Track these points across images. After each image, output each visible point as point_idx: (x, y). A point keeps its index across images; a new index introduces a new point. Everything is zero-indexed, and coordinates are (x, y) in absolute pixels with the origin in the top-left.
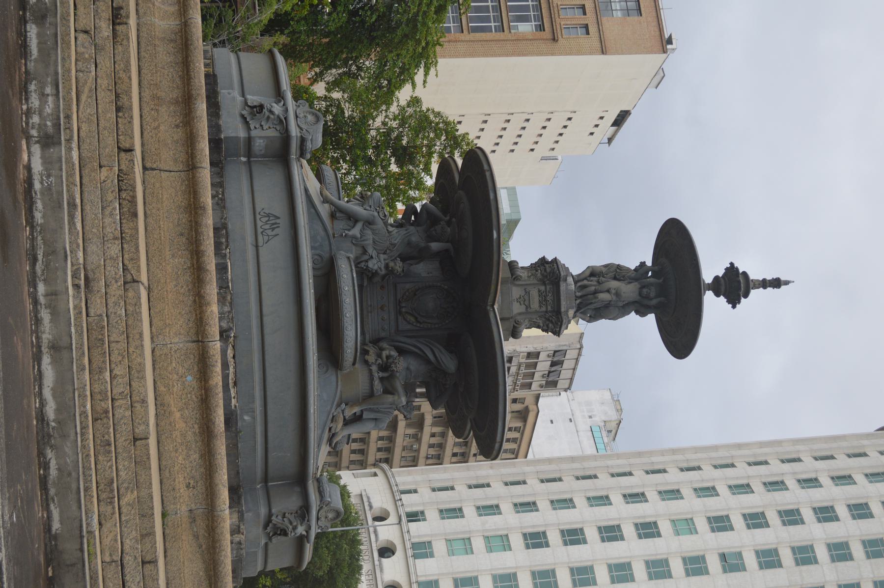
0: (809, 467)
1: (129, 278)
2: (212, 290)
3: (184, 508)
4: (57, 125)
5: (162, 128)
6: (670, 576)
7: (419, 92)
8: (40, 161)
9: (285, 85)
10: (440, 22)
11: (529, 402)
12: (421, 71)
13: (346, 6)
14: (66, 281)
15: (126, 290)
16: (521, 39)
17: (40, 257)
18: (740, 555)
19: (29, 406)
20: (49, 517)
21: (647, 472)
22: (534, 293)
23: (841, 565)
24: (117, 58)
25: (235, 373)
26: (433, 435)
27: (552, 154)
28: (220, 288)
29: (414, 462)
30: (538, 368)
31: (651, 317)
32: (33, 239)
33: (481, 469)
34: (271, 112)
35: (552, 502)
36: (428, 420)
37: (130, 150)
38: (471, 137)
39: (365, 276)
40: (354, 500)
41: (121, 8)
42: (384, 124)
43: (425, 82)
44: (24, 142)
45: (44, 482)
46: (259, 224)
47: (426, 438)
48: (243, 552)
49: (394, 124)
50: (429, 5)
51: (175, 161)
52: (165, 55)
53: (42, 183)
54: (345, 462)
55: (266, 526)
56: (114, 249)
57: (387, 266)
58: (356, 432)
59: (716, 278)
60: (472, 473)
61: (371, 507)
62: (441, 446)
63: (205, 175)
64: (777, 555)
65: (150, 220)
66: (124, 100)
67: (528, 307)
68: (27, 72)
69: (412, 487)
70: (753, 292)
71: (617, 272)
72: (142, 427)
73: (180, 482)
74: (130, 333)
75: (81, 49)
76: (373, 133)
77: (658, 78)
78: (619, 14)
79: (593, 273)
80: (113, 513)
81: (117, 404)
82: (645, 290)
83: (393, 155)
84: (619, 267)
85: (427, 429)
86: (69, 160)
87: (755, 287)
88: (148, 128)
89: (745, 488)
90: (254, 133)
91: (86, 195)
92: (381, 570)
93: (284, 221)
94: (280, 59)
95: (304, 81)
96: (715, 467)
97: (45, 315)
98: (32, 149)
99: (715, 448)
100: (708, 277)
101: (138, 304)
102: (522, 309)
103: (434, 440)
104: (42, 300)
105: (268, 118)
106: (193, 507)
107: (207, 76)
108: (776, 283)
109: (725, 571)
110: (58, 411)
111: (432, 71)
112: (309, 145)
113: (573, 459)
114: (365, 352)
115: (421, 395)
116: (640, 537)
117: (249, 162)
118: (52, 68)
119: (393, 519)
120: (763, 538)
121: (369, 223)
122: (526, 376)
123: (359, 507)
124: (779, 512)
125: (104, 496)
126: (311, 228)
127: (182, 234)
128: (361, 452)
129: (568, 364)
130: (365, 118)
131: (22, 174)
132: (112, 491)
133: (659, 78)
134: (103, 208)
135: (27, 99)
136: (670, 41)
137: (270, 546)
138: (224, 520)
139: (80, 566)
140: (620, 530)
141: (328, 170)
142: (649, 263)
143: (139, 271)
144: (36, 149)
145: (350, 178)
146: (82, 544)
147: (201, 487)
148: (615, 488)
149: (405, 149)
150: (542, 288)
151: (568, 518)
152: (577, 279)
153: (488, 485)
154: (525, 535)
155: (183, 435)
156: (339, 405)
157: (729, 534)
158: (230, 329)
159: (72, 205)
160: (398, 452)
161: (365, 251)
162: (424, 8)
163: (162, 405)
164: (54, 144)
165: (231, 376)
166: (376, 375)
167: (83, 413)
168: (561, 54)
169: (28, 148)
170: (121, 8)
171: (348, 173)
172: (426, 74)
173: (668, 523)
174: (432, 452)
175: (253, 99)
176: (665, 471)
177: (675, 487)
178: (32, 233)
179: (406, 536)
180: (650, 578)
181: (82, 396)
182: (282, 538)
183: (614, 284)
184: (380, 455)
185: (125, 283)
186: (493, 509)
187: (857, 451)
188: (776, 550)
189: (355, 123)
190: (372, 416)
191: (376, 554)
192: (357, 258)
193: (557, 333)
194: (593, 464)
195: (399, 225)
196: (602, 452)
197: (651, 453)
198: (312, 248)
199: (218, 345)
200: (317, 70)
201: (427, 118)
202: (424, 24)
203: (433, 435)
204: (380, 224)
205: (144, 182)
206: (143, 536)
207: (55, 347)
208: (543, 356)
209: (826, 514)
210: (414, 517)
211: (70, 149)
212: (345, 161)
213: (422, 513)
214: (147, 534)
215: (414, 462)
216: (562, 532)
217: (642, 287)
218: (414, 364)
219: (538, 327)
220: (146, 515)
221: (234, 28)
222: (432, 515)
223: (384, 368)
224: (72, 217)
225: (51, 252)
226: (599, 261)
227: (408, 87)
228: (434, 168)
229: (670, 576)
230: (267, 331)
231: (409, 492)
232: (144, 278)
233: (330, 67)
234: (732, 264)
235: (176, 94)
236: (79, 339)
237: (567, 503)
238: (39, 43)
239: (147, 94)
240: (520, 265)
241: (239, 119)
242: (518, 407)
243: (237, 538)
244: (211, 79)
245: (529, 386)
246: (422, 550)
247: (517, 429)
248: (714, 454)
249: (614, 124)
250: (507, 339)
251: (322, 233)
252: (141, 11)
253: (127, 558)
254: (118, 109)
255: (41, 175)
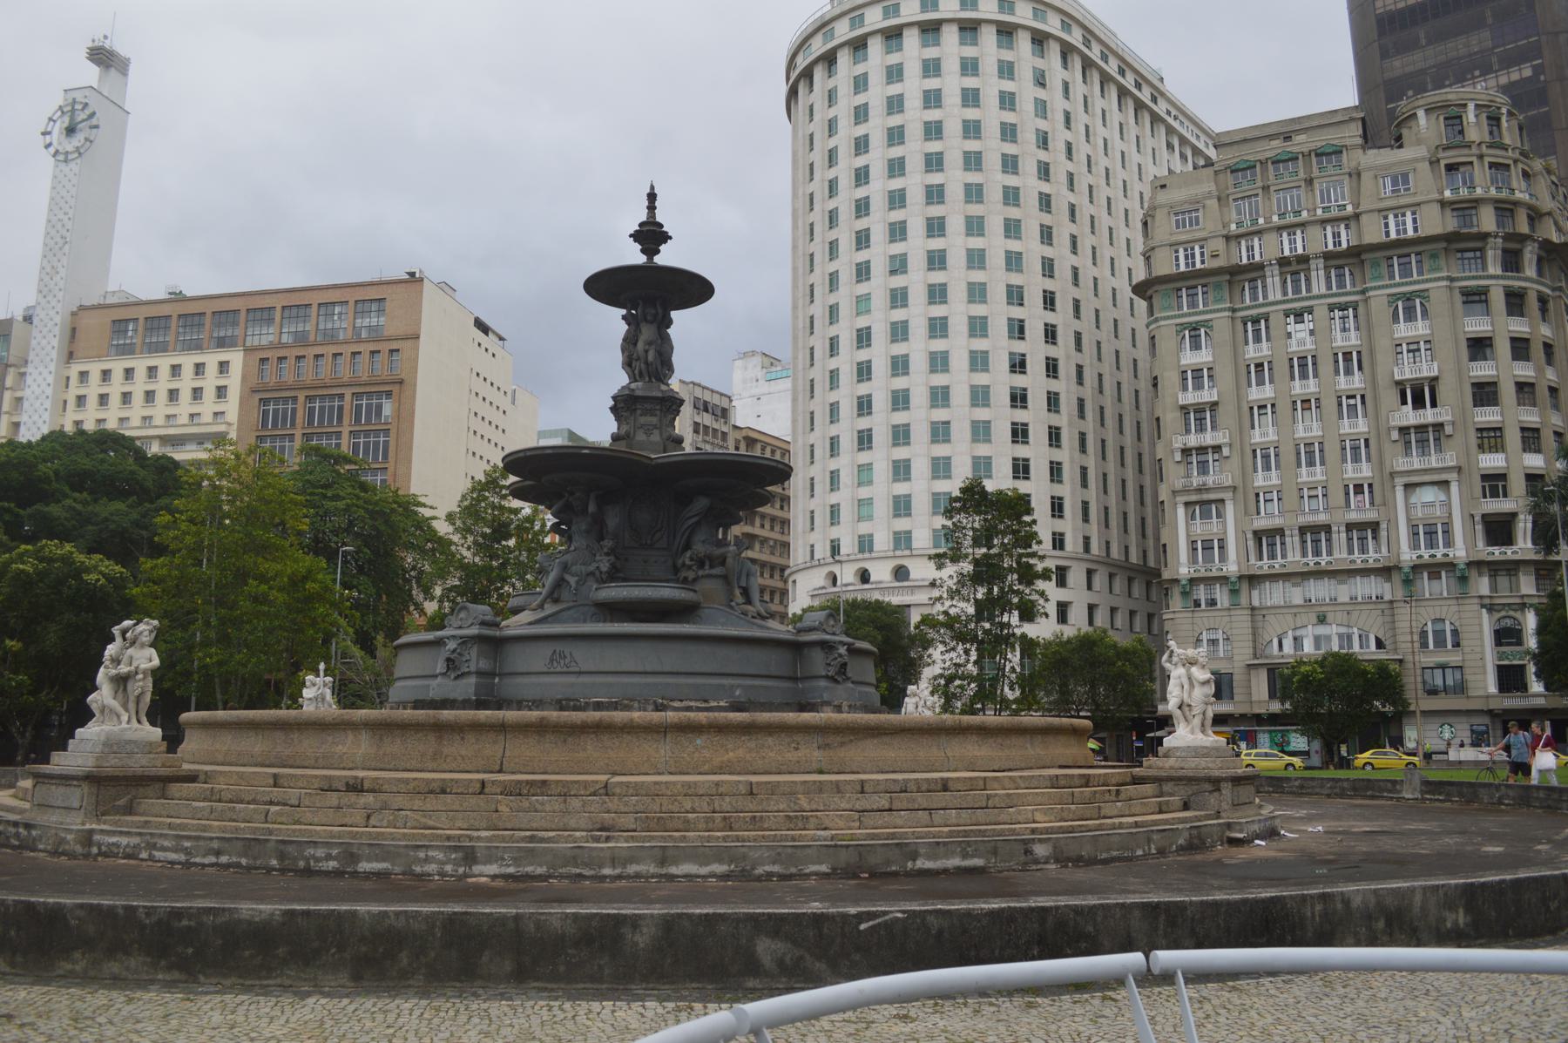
0: (819, 187)
1: (602, 791)
2: (619, 716)
3: (816, 753)
4: (456, 849)
5: (463, 753)
6: (907, 321)
7: (441, 513)
8: (488, 867)
9: (430, 636)
10: (375, 488)
11: (739, 435)
12: (421, 510)
13: (353, 576)
14: (602, 849)
15: (614, 795)
16: (398, 413)
17: (578, 871)
18: (892, 257)
19: (715, 887)
20: (816, 874)
21: (812, 333)
22: (643, 420)
23: (908, 168)
24: (395, 789)
25: (696, 700)
26: (762, 526)
27: (509, 394)
28: (616, 709)
29: (786, 545)
30: (708, 424)
31: (674, 314)
32: (562, 877)
33: (797, 484)
34: (454, 651)
35: (832, 422)
36: (748, 529)
37: (483, 783)
38: (488, 468)
39: (614, 575)
40: (816, 603)
41: (347, 784)
42: (469, 548)
43: (431, 507)
44: (470, 880)
45: (783, 877)
46: (559, 669)
47: (765, 533)
48: (858, 703)
49: (470, 539)
50: (358, 498)
51: (495, 742)
52: (394, 746)
53: (509, 866)
54: (781, 609)
55: (836, 681)
56: (575, 803)
57: (607, 554)
58: (756, 596)
59: (643, 251)
60: (800, 494)
61: (823, 588)
62: (773, 519)
63: (510, 715)
64: (894, 224)
65: (549, 769)
66: (435, 786)
67: (655, 427)
68: (404, 874)
69: (808, 549)
70: (658, 219)
71: (629, 342)
72: (741, 787)
73: (792, 756)
74: (654, 792)
75: (385, 823)
76: (477, 559)
77: (446, 289)
78: (382, 319)
79: (628, 364)
80: (817, 817)
81: (718, 809)
82: (649, 318)
83: (499, 542)
84: (625, 340)
85: (757, 531)
86: (489, 839)
87: (654, 217)
88: (462, 767)
89: (833, 247)
90: (473, 669)
91: (523, 826)
92: (881, 582)
93: (559, 646)
94: (404, 639)
95: (423, 621)
96: (812, 271)
97: (632, 869)
98: (477, 872)
99: (795, 269)
100: (641, 259)
101: (628, 784)
102: (656, 432)
103: (767, 526)
104: (618, 871)
105: (460, 654)
106: (815, 745)
107: (415, 708)
108: (652, 197)
109: (906, 272)
110: (720, 861)
111: (422, 500)
112: (488, 618)
113: (795, 400)
114: (685, 580)
115: (725, 533)
116: (869, 345)
117: (501, 675)
118: (402, 850)
119: (836, 569)
120: (879, 235)
121: (565, 568)
122: (715, 436)
123: (823, 599)
124: (857, 217)
125: (800, 825)
126: (565, 622)
127: (565, 741)
128: (772, 593)
129: (707, 397)
130: (463, 566)
131: (499, 883)
132: (796, 817)
133: (446, 288)
134: (536, 811)
135: (429, 875)
136: (412, 274)
137: (855, 679)
138: (829, 718)
139: (861, 849)
140: (862, 363)
141: (513, 602)
142: (624, 312)
143: (597, 782)
144: (477, 869)
145: (518, 584)
146: (842, 846)
147: (798, 737)
148: (824, 363)
149: (494, 531)
150: (639, 412)
151: (847, 409)
152: (633, 379)
153: (812, 479)
154: (860, 450)
155: (751, 750)
156: (732, 608)
157: (872, 265)
158: (655, 702)
159: (532, 839)
160: (775, 559)
161: (592, 574)
162: (361, 503)
163: (721, 768)
164: (473, 853)
165: (699, 704)
166: (707, 572)
167: (725, 839)
168: (416, 378)
169: (476, 876)
170: (347, 784)
171: (513, 586)
172: (424, 505)
173: (859, 318)
174: (777, 528)
175: (440, 667)
176: (812, 317)
177: (828, 309)
178: (556, 877)
179: (852, 557)
180: (906, 339)
181: (709, 839)
182: (849, 668)
183: (640, 346)
184: (777, 576)
185: (607, 795)
186: (834, 477)
187: (808, 142)
188: (890, 224)
189: (467, 575)
190: (744, 578)
191: (866, 586)
192: (597, 581)
193: (682, 402)
194: (800, 382)
195: (570, 539)
196: (790, 373)
197: (795, 328)
198: (585, 621)
199: (670, 714)
200: (412, 608)
201: (467, 508)
202: (376, 503)
203: (762, 526)
204: (568, 557)
205: (513, 773)
206: (839, 792)
207: (663, 862)
208: (698, 419)
209: (862, 176)
210: (835, 549)
211: (479, 838)
212: (502, 588)
213: (832, 541)
214: (838, 788)
215: (786, 546)
216: (859, 415)
217: (646, 320)
218: (700, 536)
219: (674, 419)
220: (820, 788)
221: (366, 683)
222: (835, 533)
223: (701, 565)
224: (542, 840)
225: (574, 861)
226: (618, 357)
227: (435, 524)
228: (515, 503)
229: (907, 321)
230: (659, 669)
231: (812, 552)
232: (603, 778)
233: (410, 595)
234: (631, 236)
235: (431, 738)
236: (657, 839)
237: (834, 408)
238: (377, 861)
239: (430, 765)
240: (615, 430)
241: (458, 682)
242: (743, 446)
243: (845, 708)
244: (418, 704)
245: (724, 434)
246: (865, 544)
247: (763, 449)
248: (801, 271)
249: (487, 334)
250: (684, 449)
251: (569, 612)
252: (351, 765)
253: (858, 807)
254: (443, 792)
255: (502, 865)
